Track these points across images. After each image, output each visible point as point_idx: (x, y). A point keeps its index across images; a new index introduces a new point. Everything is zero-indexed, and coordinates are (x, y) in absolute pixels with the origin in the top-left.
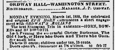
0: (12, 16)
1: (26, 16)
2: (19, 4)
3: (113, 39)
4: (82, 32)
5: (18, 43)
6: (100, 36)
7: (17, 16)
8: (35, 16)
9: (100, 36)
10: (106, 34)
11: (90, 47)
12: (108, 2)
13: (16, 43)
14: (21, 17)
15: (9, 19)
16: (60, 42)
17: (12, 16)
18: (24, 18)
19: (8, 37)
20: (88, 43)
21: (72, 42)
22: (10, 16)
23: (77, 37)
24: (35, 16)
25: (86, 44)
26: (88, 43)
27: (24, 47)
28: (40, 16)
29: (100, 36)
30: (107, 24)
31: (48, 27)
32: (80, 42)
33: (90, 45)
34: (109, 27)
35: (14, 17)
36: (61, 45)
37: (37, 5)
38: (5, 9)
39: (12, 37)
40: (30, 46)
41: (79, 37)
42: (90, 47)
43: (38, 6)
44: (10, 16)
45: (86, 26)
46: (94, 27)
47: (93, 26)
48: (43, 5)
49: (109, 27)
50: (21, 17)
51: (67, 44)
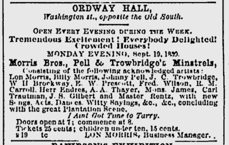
0: (52, 52)
1: (76, 30)
2: (117, 134)
3: (4, 120)
4: (107, 96)
7: (61, 52)
8: (93, 30)
10: (186, 91)
11: (44, 139)
12: (13, 139)
14: (70, 54)
17: (52, 52)
18: (77, 56)
22: (49, 52)
24: (93, 30)
28: (100, 31)
31: (114, 91)
32: (158, 128)
33: (42, 134)
34: (158, 117)
37: (171, 83)
38: (140, 4)
39: (45, 40)
40: (41, 110)
42: (44, 139)
43: (170, 81)
44: (49, 52)
45: (95, 71)
46: (65, 52)
47: (98, 32)
48: (142, 10)
49: (182, 18)
50: (70, 54)
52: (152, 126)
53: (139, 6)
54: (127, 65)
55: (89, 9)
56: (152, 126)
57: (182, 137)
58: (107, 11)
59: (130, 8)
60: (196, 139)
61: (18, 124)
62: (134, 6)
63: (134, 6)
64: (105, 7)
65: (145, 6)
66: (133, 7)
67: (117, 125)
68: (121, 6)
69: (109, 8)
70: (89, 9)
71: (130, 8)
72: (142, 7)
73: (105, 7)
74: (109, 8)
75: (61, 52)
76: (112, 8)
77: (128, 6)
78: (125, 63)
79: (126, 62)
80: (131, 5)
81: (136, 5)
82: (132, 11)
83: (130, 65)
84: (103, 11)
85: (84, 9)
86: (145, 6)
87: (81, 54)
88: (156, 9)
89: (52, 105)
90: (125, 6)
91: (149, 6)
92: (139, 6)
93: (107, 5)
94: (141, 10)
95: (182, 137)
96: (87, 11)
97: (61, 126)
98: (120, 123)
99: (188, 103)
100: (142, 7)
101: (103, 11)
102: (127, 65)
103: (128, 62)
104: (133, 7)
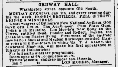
0: (12, 13)
5: (8, 47)
6: (103, 25)
7: (16, 13)
9: (103, 26)
11: (38, 65)
13: (16, 60)
15: (8, 15)
16: (33, 9)
19: (40, 5)
20: (89, 59)
21: (80, 22)
22: (10, 13)
23: (98, 17)
25: (98, 61)
26: (89, 59)
27: (90, 47)
29: (103, 26)
30: (22, 8)
32: (81, 58)
34: (110, 16)
35: (14, 14)
36: (69, 35)
38: (73, 2)
41: (100, 17)
42: (38, 65)
44: (10, 13)
48: (74, 6)
49: (110, 16)
50: (20, 14)
51: (107, 44)
52: (78, 58)
53: (73, 3)
54: (50, 5)
55: (47, 5)
56: (78, 58)
57: (94, 63)
58: (56, 6)
59: (68, 4)
60: (100, 64)
61: (10, 58)
62: (70, 3)
63: (70, 3)
64: (55, 4)
65: (76, 3)
66: (70, 4)
67: (20, 52)
68: (63, 3)
69: (57, 5)
70: (47, 5)
71: (68, 4)
72: (74, 4)
73: (55, 4)
74: (57, 5)
75: (16, 13)
76: (59, 5)
77: (67, 3)
78: (49, 4)
79: (49, 3)
80: (68, 3)
81: (71, 3)
82: (69, 6)
83: (52, 5)
84: (54, 6)
85: (44, 5)
86: (76, 3)
87: (59, 5)
88: (80, 5)
89: (89, 63)
90: (65, 3)
91: (78, 3)
92: (73, 3)
93: (56, 3)
94: (73, 5)
95: (94, 63)
96: (46, 6)
97: (32, 59)
98: (22, 51)
99: (101, 45)
100: (74, 4)
101: (54, 6)
102: (50, 5)
103: (51, 3)
104: (70, 4)
